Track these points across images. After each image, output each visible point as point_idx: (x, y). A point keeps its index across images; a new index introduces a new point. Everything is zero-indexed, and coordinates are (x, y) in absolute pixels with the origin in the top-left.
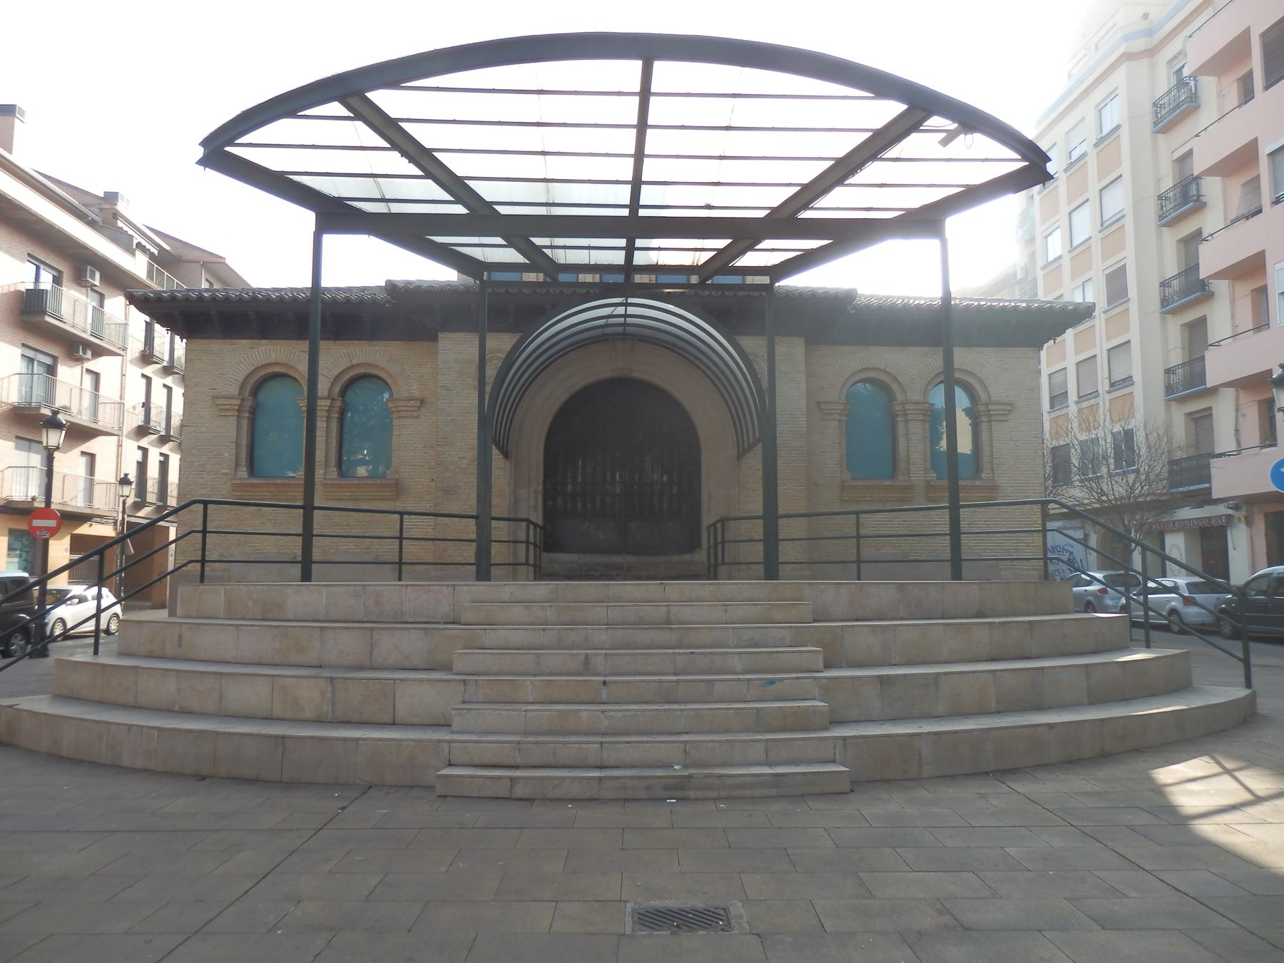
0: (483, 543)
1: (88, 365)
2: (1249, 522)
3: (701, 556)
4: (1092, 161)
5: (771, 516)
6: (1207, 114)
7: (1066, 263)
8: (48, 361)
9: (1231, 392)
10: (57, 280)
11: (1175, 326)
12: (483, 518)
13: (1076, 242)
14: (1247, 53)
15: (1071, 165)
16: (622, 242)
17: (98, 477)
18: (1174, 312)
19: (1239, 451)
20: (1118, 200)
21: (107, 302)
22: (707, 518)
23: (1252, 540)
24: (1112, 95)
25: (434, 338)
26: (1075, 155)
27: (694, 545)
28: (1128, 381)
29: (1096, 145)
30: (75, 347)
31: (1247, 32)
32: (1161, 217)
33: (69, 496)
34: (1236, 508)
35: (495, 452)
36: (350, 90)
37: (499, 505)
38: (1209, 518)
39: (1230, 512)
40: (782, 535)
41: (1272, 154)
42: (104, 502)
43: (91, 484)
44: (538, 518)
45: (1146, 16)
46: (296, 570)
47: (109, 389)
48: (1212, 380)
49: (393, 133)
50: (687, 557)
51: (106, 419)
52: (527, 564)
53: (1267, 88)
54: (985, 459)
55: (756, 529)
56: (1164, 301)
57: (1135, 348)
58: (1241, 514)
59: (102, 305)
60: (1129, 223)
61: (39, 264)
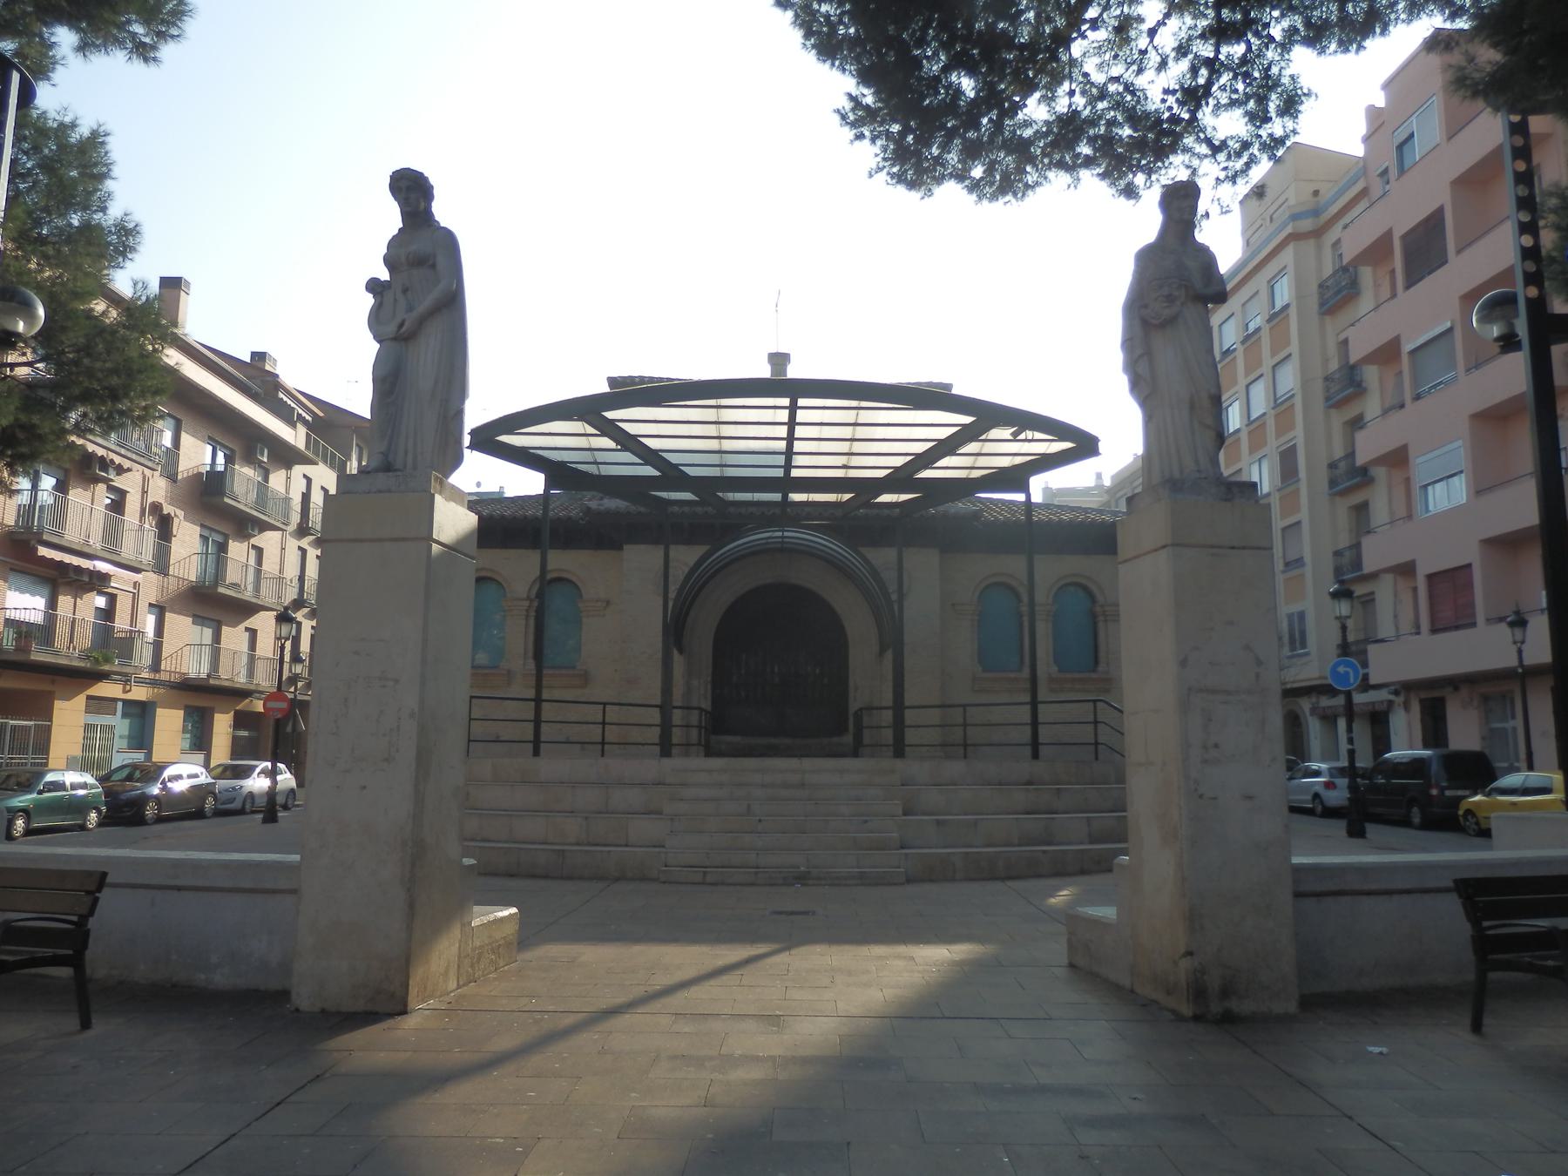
0: (666, 727)
1: (253, 541)
2: (1407, 706)
3: (848, 739)
4: (1240, 355)
5: (899, 706)
6: (1366, 302)
7: (1244, 436)
8: (220, 539)
9: (1389, 578)
10: (229, 460)
11: (1343, 506)
12: (665, 708)
13: (1254, 416)
14: (1391, 251)
15: (1248, 337)
16: (786, 402)
17: (259, 652)
18: (1343, 493)
19: (1398, 637)
20: (1288, 379)
21: (272, 477)
22: (853, 706)
23: (1409, 724)
24: (1281, 272)
25: (620, 548)
26: (1251, 330)
27: (841, 729)
28: (1299, 562)
29: (1269, 321)
30: (245, 525)
31: (1389, 234)
32: (1327, 399)
33: (234, 673)
34: (1396, 693)
35: (675, 652)
36: (585, 409)
37: (677, 698)
38: (1373, 703)
39: (1392, 697)
40: (908, 722)
41: (1413, 352)
42: (265, 680)
43: (252, 659)
44: (706, 704)
45: (1316, 193)
46: (1028, 751)
47: (270, 565)
48: (1369, 566)
49: (610, 429)
50: (835, 739)
51: (267, 596)
52: (699, 744)
53: (1407, 287)
54: (1102, 654)
55: (887, 717)
56: (1333, 483)
57: (1306, 527)
58: (1400, 700)
59: (266, 479)
60: (1298, 401)
61: (216, 445)
